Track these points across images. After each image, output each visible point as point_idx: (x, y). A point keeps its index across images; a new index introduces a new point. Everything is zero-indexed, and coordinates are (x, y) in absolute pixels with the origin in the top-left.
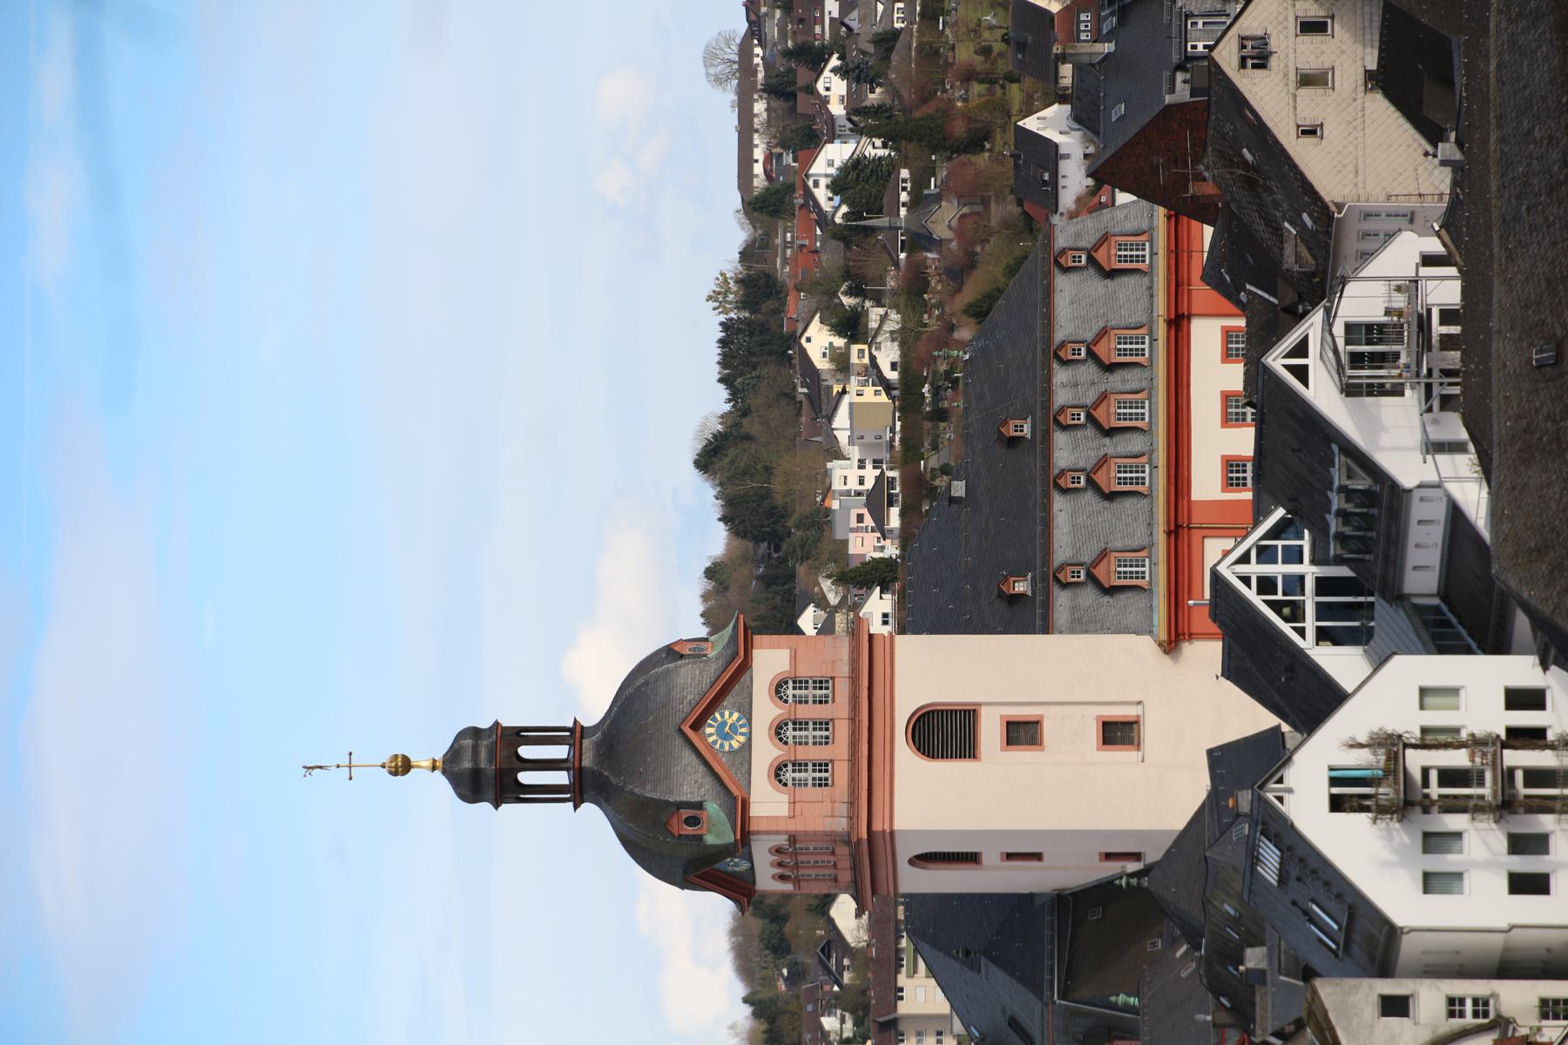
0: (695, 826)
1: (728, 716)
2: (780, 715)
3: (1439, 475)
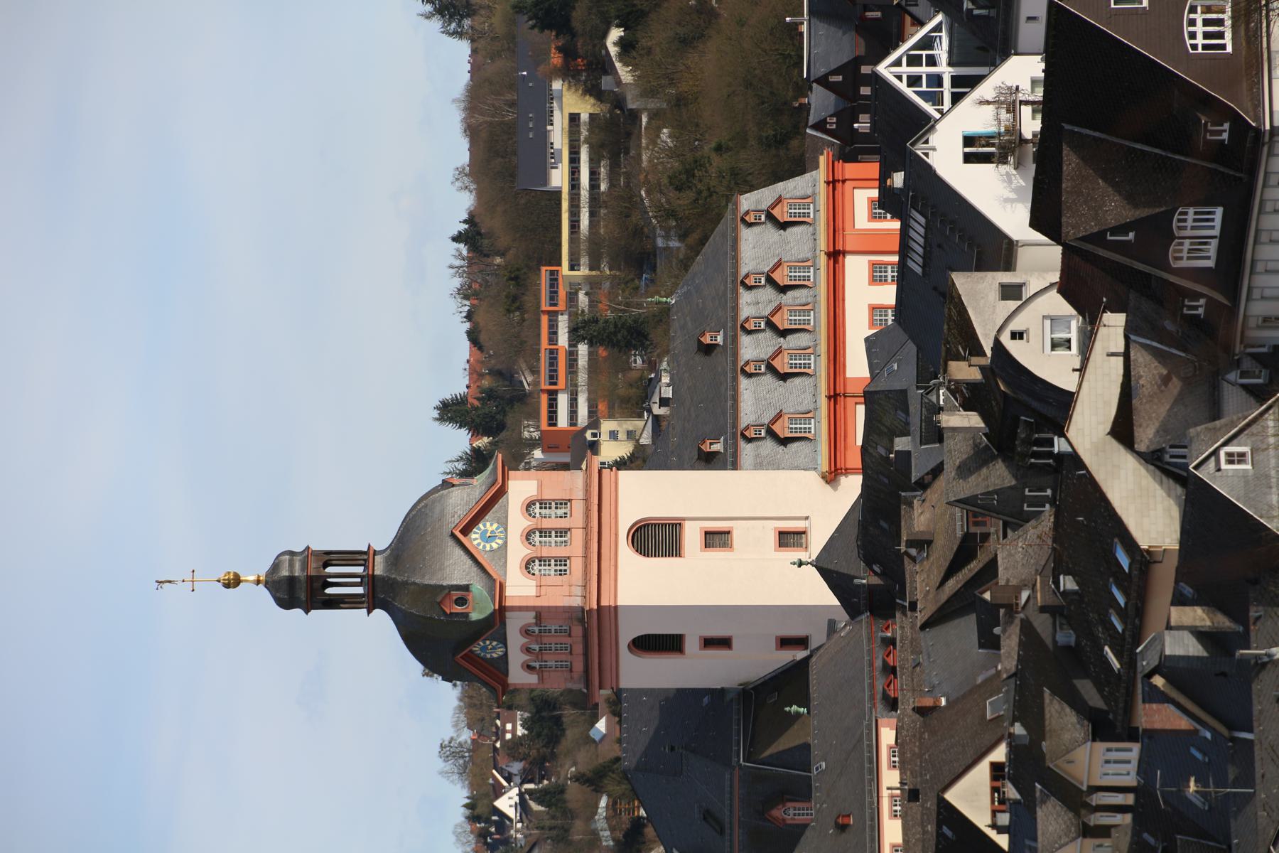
1: (488, 525)
2: (529, 525)
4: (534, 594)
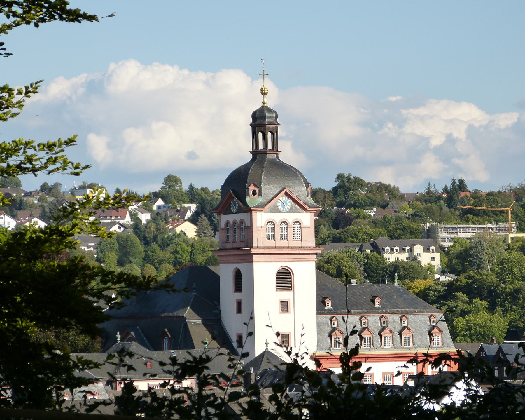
0: (252, 194)
4: (258, 225)
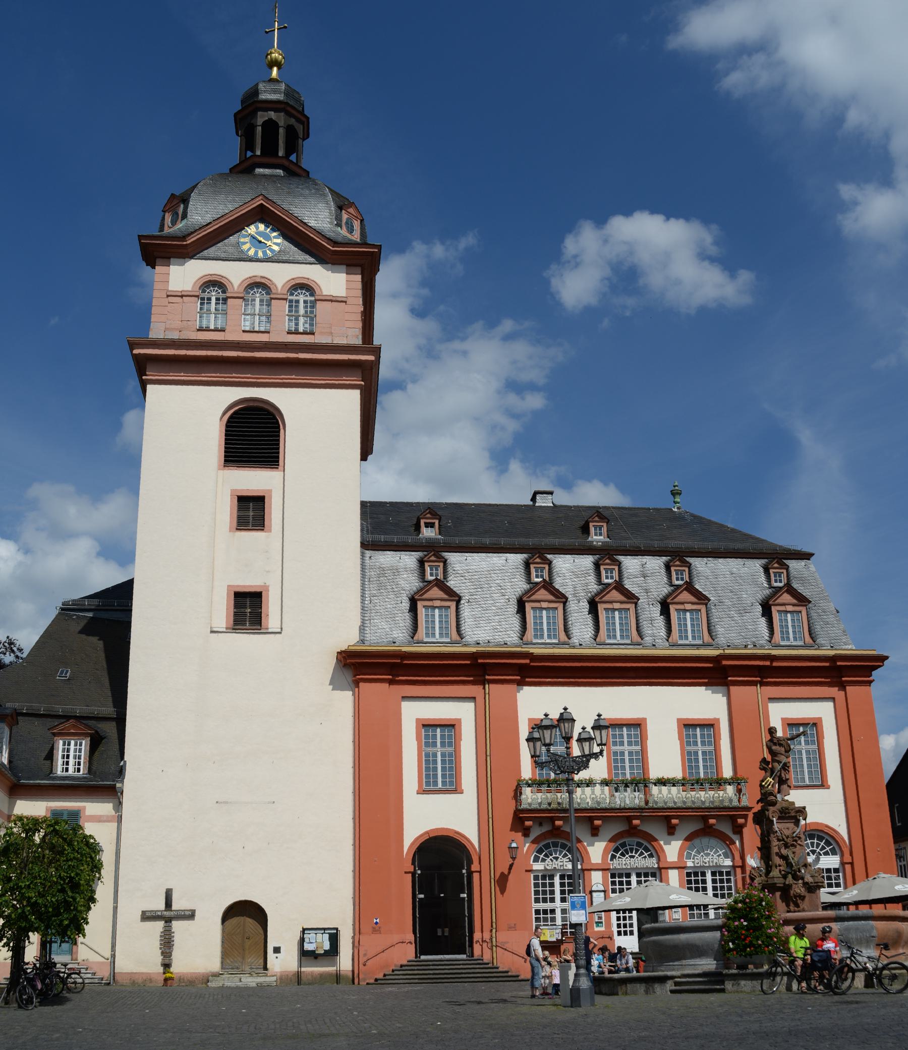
1: (276, 242)
3: (167, 966)
